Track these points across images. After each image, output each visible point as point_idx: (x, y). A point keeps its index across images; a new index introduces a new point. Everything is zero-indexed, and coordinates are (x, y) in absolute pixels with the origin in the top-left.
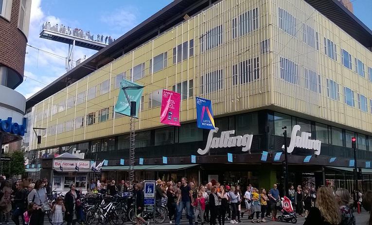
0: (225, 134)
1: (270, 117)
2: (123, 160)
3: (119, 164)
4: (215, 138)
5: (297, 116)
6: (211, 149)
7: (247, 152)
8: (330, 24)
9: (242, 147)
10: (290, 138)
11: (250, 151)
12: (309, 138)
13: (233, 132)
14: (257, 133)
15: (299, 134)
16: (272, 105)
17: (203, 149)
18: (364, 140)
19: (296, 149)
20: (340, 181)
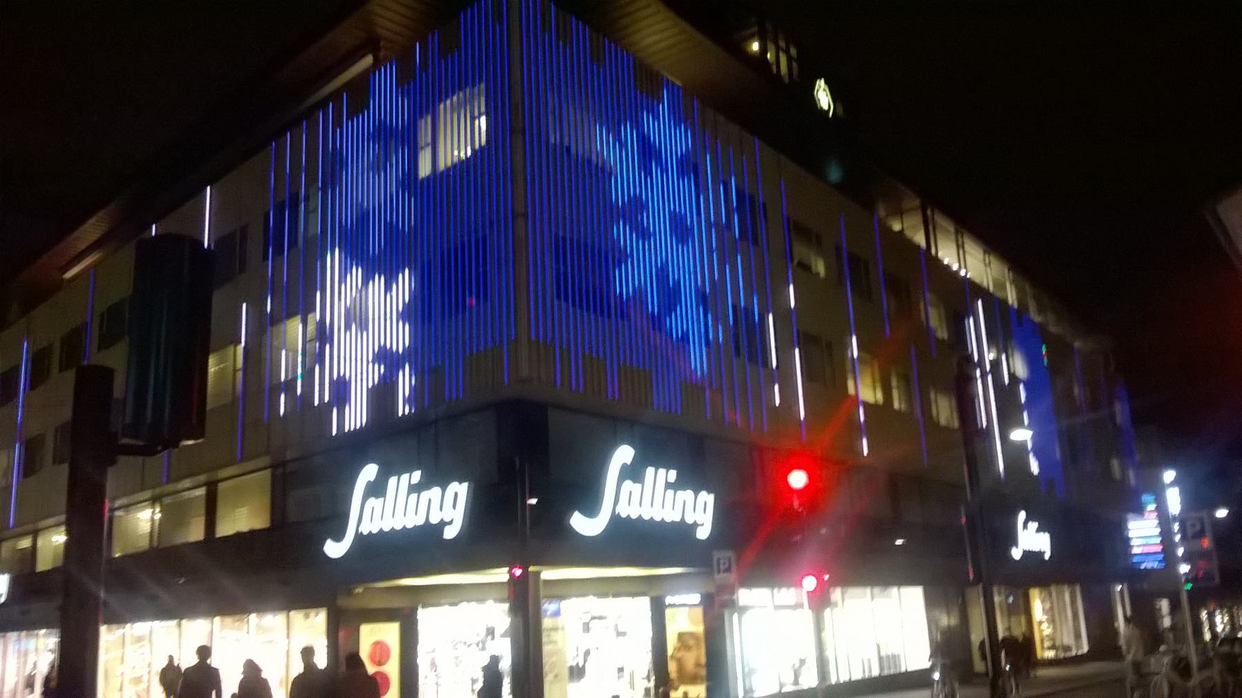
0: (399, 484)
4: (372, 502)
9: (443, 524)
12: (668, 486)
13: (417, 476)
19: (615, 519)
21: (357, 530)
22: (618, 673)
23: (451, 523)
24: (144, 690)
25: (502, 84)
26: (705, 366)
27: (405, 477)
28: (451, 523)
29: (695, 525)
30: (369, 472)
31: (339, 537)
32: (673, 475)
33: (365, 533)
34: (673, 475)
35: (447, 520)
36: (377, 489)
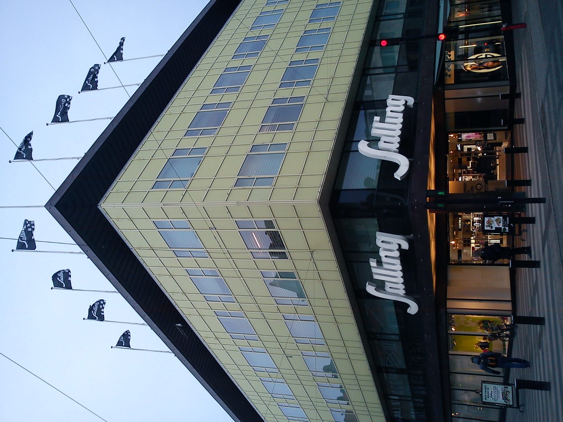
0: (378, 273)
1: (343, 199)
2: (518, 224)
3: (504, 333)
4: (387, 289)
6: (409, 293)
7: (410, 242)
9: (400, 249)
11: (408, 237)
12: (382, 121)
13: (373, 263)
15: (374, 142)
16: (321, 202)
17: (408, 306)
19: (402, 150)
21: (408, 72)
23: (400, 245)
24: (171, 188)
25: (544, 369)
27: (374, 270)
28: (400, 245)
29: (406, 105)
30: (371, 289)
32: (377, 118)
33: (404, 292)
34: (377, 118)
35: (397, 247)
36: (380, 286)
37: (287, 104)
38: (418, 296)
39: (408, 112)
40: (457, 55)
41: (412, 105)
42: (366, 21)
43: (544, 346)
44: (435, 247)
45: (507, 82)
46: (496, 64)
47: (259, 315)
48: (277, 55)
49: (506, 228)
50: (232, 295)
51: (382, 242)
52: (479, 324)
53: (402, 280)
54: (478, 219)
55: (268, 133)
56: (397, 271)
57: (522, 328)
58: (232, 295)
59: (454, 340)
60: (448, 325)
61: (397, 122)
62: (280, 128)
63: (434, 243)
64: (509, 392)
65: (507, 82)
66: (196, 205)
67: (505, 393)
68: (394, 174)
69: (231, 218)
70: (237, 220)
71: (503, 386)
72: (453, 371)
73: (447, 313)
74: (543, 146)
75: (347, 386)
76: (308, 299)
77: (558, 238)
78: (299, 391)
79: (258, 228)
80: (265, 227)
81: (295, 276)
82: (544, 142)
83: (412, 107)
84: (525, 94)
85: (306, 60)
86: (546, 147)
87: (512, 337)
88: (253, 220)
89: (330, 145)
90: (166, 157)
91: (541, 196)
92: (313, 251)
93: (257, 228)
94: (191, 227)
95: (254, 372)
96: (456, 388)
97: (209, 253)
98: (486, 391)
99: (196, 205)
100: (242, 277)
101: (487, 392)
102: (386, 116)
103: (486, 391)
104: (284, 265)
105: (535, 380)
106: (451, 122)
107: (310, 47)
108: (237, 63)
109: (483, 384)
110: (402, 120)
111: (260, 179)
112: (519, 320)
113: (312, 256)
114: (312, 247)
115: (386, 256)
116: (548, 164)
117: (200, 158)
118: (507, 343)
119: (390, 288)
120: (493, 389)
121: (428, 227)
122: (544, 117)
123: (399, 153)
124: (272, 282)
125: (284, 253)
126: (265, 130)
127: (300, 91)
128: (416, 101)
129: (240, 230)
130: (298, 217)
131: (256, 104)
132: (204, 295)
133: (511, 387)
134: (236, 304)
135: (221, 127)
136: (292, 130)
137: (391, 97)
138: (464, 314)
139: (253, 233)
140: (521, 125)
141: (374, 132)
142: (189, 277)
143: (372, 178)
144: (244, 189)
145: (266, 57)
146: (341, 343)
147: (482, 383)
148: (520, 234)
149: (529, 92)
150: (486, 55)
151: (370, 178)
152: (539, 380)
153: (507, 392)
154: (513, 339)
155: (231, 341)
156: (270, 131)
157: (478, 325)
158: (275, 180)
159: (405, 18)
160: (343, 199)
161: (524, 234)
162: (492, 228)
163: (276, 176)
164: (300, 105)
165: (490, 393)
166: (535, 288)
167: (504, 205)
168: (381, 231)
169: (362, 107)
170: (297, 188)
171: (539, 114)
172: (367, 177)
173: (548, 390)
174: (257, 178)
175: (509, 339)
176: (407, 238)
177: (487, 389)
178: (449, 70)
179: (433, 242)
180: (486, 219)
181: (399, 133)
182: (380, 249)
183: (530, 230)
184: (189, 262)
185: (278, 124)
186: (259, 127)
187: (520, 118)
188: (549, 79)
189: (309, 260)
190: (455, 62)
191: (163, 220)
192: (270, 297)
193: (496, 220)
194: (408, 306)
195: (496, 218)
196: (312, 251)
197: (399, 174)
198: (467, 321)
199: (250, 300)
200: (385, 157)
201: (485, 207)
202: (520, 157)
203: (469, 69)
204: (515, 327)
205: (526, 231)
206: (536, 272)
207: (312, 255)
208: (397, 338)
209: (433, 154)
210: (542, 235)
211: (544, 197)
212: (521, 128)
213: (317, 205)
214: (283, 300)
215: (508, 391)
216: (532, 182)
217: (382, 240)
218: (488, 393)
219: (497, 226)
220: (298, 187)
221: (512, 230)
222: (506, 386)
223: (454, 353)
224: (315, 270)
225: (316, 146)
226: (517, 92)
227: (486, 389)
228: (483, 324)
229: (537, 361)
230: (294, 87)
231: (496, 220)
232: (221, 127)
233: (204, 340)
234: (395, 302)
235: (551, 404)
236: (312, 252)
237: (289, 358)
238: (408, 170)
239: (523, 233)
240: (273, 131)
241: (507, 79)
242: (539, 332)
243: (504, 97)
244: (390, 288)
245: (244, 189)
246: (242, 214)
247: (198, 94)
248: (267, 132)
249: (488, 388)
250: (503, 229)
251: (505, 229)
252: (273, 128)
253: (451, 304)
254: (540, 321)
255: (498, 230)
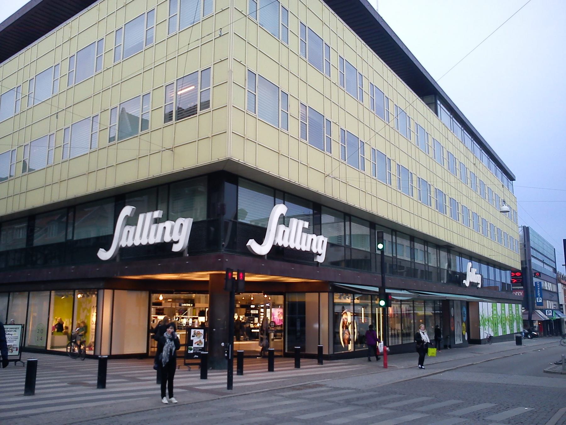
0: (145, 219)
1: (228, 187)
4: (128, 228)
5: (286, 190)
6: (122, 251)
7: (180, 253)
8: (464, 246)
9: (172, 243)
10: (266, 229)
12: (304, 230)
13: (157, 214)
14: (202, 216)
15: (284, 220)
16: (229, 161)
17: (107, 249)
18: (407, 243)
20: (251, 316)
22: (208, 102)
26: (289, 368)
27: (149, 215)
29: (318, 254)
30: (127, 211)
31: (107, 249)
32: (306, 225)
34: (306, 225)
35: (175, 240)
36: (131, 221)
37: (325, 135)
38: (118, 260)
39: (309, 256)
40: (344, 306)
41: (316, 260)
42: (395, 220)
43: (74, 388)
44: (171, 279)
45: (331, 352)
46: (346, 341)
47: (99, 88)
48: (386, 124)
49: (192, 351)
50: (123, 59)
51: (182, 224)
52: (83, 322)
53: (137, 244)
54: (190, 323)
55: (299, 112)
56: (148, 239)
57: (94, 365)
58: (123, 59)
59: (67, 296)
60: (85, 291)
61: (302, 244)
62: (304, 125)
63: (175, 279)
64: (12, 352)
65: (331, 352)
66: (230, 24)
67: (10, 349)
68: (253, 240)
69: (214, 63)
70: (212, 69)
71: (18, 346)
72: (30, 295)
73: (98, 289)
74: (283, 387)
75: (12, 183)
76: (116, 143)
77: (197, 402)
78: (42, 111)
79: (201, 92)
80: (111, 137)
81: (144, 130)
82: (287, 388)
83: (315, 260)
84: (323, 369)
85: (364, 158)
86: (283, 389)
87: (73, 355)
88: (211, 87)
89: (284, 176)
90: (164, 57)
91: (234, 385)
92: (172, 151)
93: (201, 91)
94: (205, 17)
95: (16, 86)
96: (11, 298)
97: (191, 28)
98: (12, 328)
99: (230, 24)
100: (178, 56)
101: (11, 330)
102: (308, 234)
103: (12, 328)
104: (157, 119)
105: (37, 379)
106: (296, 298)
107: (376, 163)
108: (366, 87)
109: (21, 326)
110: (303, 249)
111: (254, 98)
112: (103, 364)
113: (167, 149)
114: (176, 150)
115: (165, 228)
116: (267, 391)
117: (278, 36)
118: (64, 350)
119: (129, 231)
120: (14, 336)
121: (197, 271)
122: (310, 387)
123: (273, 246)
124: (125, 111)
125: (171, 119)
126: (302, 110)
127: (336, 149)
128: (320, 264)
129: (200, 73)
130: (212, 136)
131: (327, 102)
132: (76, 56)
133: (17, 354)
134: (113, 64)
135: (308, 62)
136: (301, 138)
137: (326, 240)
138: (97, 306)
139: (193, 87)
140: (294, 365)
141: (294, 222)
142: (97, 41)
143: (247, 216)
144: (245, 80)
145: (368, 117)
146: (64, 177)
147: (22, 325)
148: (186, 364)
149: (327, 372)
150: (464, 327)
151: (247, 215)
152: (36, 382)
153: (12, 350)
154: (68, 356)
155: (66, 55)
156: (301, 115)
157: (81, 321)
158: (253, 114)
159: (393, 257)
160: (228, 187)
161: (186, 368)
162: (193, 336)
163: (256, 116)
164: (323, 148)
165: (11, 333)
166: (133, 379)
167: (227, 349)
168: (193, 223)
169: (315, 212)
170: (244, 138)
171: (311, 382)
172: (247, 211)
173: (25, 392)
174: (255, 95)
175: (69, 352)
176: (184, 250)
177: (15, 330)
178: (345, 298)
179: (179, 277)
180: (202, 331)
181: (292, 247)
182: (173, 222)
183: (189, 374)
184: (65, 68)
185: (307, 123)
186: (305, 104)
187: (301, 364)
188: (350, 391)
189: (162, 145)
190: (352, 304)
191: (155, 20)
192: (72, 123)
193: (200, 341)
194: (107, 249)
195: (203, 341)
196: (173, 150)
197: (252, 244)
198: (86, 310)
199: (117, 80)
200: (270, 231)
201: (214, 330)
202: (151, 366)
203: (344, 316)
204: (83, 358)
205: (189, 370)
206: (153, 380)
207: (169, 149)
208: (70, 237)
209: (266, 280)
210: (193, 386)
211: (233, 388)
212: (290, 365)
213: (226, 157)
214: (116, 116)
215: (13, 351)
216: (241, 376)
217: (183, 225)
218: (10, 331)
219: (194, 342)
220: (245, 138)
221: (191, 356)
222: (18, 349)
223: (53, 297)
224: (150, 152)
225: (284, 160)
226: (324, 361)
227: (15, 328)
228: (83, 326)
229: (54, 381)
230: (340, 143)
231: (200, 341)
232: (308, 62)
233: (68, 25)
234: (112, 236)
235: (10, 397)
236: (171, 149)
237: (56, 115)
238: (256, 253)
239: (187, 367)
240: (301, 117)
241: (334, 352)
242: (87, 383)
243: (320, 349)
244: (129, 231)
245: (245, 80)
246: (218, 74)
247: (340, 42)
248: (300, 111)
249: (16, 331)
250: (191, 348)
251: (191, 350)
252: (304, 117)
253: (108, 294)
254: (102, 383)
255: (190, 343)
